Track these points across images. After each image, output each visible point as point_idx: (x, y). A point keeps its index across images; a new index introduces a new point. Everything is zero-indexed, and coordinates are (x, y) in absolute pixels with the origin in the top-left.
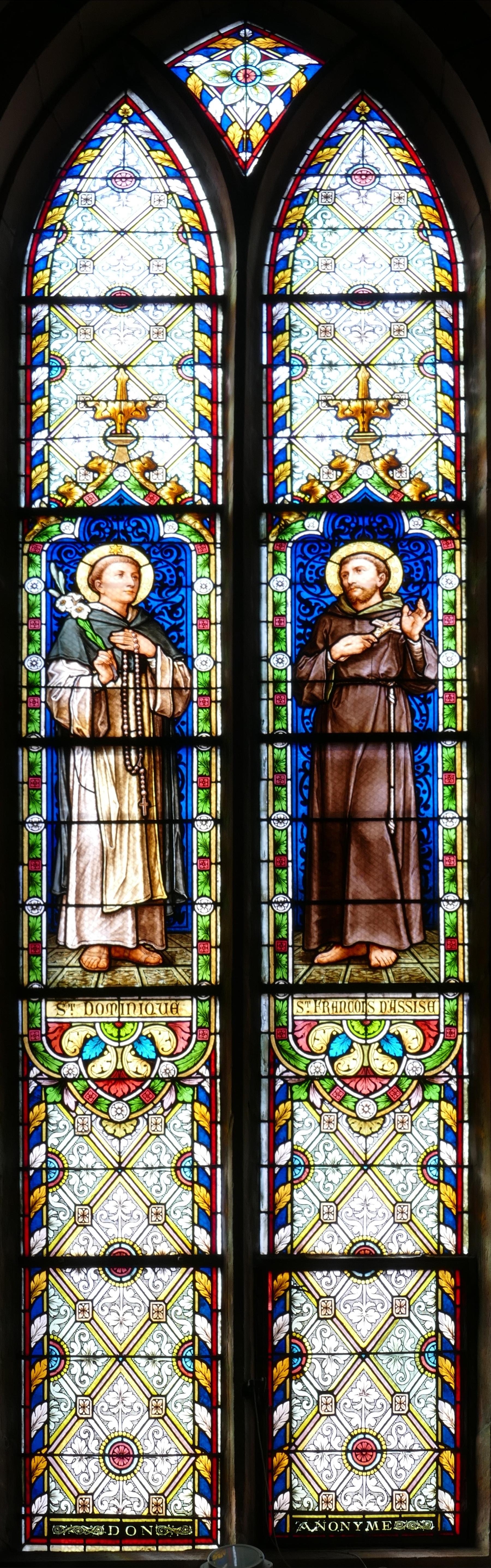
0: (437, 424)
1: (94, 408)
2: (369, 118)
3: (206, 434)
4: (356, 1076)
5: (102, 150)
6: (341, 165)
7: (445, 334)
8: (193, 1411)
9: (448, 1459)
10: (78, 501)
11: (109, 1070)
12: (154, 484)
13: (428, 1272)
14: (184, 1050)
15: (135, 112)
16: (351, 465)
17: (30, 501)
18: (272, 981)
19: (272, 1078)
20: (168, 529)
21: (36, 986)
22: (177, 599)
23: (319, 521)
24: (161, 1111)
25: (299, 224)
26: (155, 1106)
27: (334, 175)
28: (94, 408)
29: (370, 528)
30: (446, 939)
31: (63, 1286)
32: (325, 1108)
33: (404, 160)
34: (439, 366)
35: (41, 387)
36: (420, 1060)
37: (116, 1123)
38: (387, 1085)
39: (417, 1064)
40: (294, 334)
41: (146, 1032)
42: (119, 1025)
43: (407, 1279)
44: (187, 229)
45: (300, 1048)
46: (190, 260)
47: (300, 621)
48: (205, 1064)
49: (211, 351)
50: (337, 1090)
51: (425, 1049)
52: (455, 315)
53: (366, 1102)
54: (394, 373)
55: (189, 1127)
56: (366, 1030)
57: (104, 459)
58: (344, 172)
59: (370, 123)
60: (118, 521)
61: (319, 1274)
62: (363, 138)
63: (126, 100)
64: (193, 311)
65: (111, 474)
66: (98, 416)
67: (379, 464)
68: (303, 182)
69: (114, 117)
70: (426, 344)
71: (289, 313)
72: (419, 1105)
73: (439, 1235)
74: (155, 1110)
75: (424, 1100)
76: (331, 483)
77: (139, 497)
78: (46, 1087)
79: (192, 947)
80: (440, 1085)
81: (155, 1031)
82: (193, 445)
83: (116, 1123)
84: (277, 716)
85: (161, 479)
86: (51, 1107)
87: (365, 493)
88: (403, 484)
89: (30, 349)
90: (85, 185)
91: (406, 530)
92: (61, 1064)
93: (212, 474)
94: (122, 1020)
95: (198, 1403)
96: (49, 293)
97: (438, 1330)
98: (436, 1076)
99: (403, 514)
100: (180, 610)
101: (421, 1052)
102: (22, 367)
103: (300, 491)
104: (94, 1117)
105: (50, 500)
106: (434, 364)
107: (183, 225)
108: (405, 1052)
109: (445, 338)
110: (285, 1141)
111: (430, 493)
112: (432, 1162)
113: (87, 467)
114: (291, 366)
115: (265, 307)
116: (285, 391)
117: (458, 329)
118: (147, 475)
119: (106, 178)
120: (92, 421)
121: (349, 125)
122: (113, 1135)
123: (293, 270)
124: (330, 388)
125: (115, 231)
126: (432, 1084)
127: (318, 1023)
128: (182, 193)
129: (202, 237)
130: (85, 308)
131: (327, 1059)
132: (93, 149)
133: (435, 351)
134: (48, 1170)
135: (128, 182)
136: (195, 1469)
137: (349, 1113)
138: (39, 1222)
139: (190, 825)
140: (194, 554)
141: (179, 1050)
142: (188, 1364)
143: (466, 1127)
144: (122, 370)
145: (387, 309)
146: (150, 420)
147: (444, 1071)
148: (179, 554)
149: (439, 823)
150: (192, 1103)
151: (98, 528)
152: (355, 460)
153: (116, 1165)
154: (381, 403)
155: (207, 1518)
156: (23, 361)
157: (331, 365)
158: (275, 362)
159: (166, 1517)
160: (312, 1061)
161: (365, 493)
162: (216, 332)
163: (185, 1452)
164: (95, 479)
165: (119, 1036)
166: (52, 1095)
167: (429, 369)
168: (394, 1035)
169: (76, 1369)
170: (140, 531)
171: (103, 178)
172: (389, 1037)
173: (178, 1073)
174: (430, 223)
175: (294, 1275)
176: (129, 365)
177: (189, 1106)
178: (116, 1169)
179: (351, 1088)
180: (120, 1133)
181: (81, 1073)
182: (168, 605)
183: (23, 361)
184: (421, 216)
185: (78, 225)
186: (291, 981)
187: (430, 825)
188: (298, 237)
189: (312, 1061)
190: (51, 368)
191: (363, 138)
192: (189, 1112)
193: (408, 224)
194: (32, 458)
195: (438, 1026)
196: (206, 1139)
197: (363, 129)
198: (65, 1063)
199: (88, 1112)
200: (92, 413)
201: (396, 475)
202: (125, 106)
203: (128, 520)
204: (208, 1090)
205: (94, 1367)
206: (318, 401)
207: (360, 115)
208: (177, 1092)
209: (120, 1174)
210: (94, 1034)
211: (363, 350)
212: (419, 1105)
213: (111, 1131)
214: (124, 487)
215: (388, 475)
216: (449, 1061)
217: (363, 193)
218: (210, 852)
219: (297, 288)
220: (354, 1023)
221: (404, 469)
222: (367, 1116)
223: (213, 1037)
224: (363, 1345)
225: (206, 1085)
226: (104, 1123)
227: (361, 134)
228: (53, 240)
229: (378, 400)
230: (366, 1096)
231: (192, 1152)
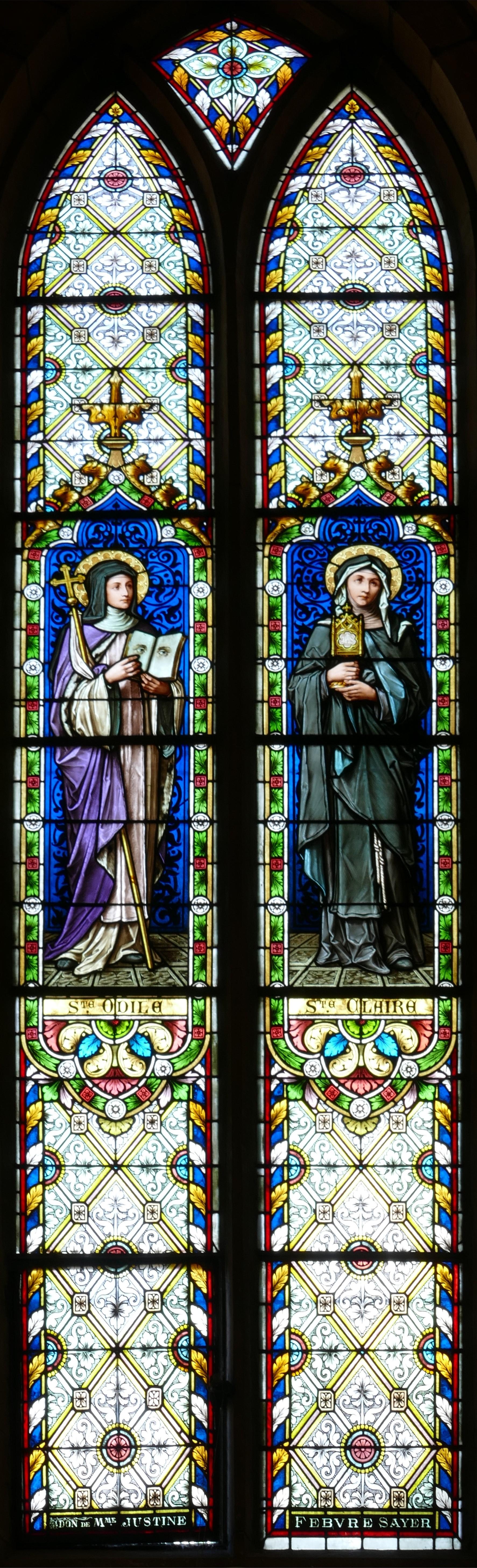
0: (188, 429)
1: (89, 412)
2: (358, 116)
3: (441, 432)
4: (103, 1078)
5: (93, 150)
6: (330, 164)
7: (437, 334)
8: (434, 1403)
9: (199, 1452)
10: (74, 504)
11: (351, 1068)
12: (391, 483)
13: (176, 1270)
14: (179, 1048)
15: (361, 107)
16: (344, 467)
17: (25, 504)
18: (268, 982)
19: (269, 1078)
20: (407, 530)
21: (31, 985)
22: (174, 602)
23: (314, 526)
24: (402, 1109)
25: (289, 224)
26: (396, 1104)
27: (87, 178)
28: (89, 412)
29: (366, 534)
30: (195, 942)
31: (306, 1279)
32: (75, 1109)
33: (393, 159)
34: (431, 367)
35: (276, 385)
36: (415, 1061)
37: (361, 1121)
38: (382, 1085)
39: (412, 1064)
40: (48, 338)
41: (141, 1030)
42: (360, 1023)
43: (157, 1277)
44: (179, 228)
45: (50, 1048)
46: (183, 260)
47: (297, 626)
48: (200, 1062)
49: (445, 348)
50: (87, 1090)
51: (420, 1049)
52: (446, 315)
53: (116, 1102)
54: (145, 378)
55: (184, 1125)
56: (361, 1030)
57: (99, 462)
58: (334, 171)
59: (359, 122)
60: (116, 525)
61: (73, 1271)
62: (352, 137)
63: (116, 100)
64: (426, 310)
65: (348, 475)
66: (93, 420)
67: (372, 465)
68: (56, 185)
69: (105, 117)
70: (418, 344)
71: (282, 313)
72: (169, 1104)
73: (189, 1234)
74: (151, 1108)
75: (173, 1099)
76: (83, 488)
77: (133, 499)
78: (42, 1086)
79: (189, 948)
80: (189, 1085)
81: (397, 1029)
82: (187, 447)
83: (357, 1120)
84: (272, 718)
85: (156, 482)
86: (47, 1105)
87: (117, 499)
88: (395, 485)
89: (263, 348)
90: (81, 186)
91: (401, 535)
92: (302, 1061)
93: (448, 472)
94: (364, 1017)
95: (440, 1394)
96: (44, 294)
97: (436, 1325)
98: (183, 1076)
99: (398, 519)
100: (177, 614)
101: (416, 1052)
102: (257, 366)
103: (294, 492)
104: (335, 1114)
105: (288, 499)
106: (426, 365)
107: (174, 225)
108: (154, 1052)
109: (436, 338)
110: (281, 1140)
111: (181, 498)
112: (428, 1161)
113: (81, 470)
114: (45, 370)
115: (257, 307)
116: (276, 391)
117: (260, 332)
118: (141, 478)
119: (99, 178)
120: (86, 425)
121: (340, 124)
122: (108, 1133)
123: (284, 269)
124: (83, 392)
125: (346, 227)
126: (181, 1084)
127: (66, 1023)
128: (410, 188)
129: (193, 237)
130: (316, 305)
131: (76, 1059)
132: (85, 149)
133: (187, 356)
134: (289, 1167)
135: (120, 182)
136: (192, 1459)
137: (345, 1113)
138: (35, 1218)
139: (430, 825)
140: (191, 558)
141: (175, 1048)
142: (429, 1357)
143: (215, 1126)
144: (116, 373)
145: (140, 314)
146: (144, 423)
147: (193, 1070)
148: (418, 555)
149: (190, 826)
150: (188, 1101)
151: (339, 529)
152: (348, 462)
153: (111, 1163)
154: (374, 404)
155: (202, 1507)
156: (257, 359)
157: (387, 365)
158: (30, 367)
159: (163, 1508)
160: (61, 1061)
161: (117, 499)
162: (450, 330)
163: (425, 1444)
164: (90, 483)
165: (361, 1033)
166: (49, 1093)
167: (181, 374)
168: (142, 1035)
169: (318, 1363)
170: (138, 536)
171: (331, 175)
172: (384, 1036)
173: (174, 1071)
174: (181, 225)
175: (48, 1272)
176: (124, 368)
177: (184, 1104)
178: (357, 1167)
179: (100, 1089)
180: (115, 1130)
181: (77, 1073)
182: (165, 610)
183: (257, 359)
184: (173, 219)
185: (309, 223)
186: (41, 982)
187: (181, 827)
188: (289, 236)
189: (61, 1061)
190: (285, 365)
191: (352, 137)
192: (183, 1110)
193: (397, 221)
194: (269, 457)
195: (432, 1025)
196: (447, 1137)
197: (352, 128)
198: (307, 1060)
199: (330, 1110)
200: (86, 417)
201: (147, 480)
202: (116, 106)
203: (127, 525)
204: (203, 1087)
205: (335, 1360)
206: (71, 405)
207: (349, 114)
208: (173, 1091)
209: (116, 1172)
210: (336, 1031)
211: (116, 356)
212: (169, 1104)
213: (107, 1129)
214: (361, 487)
215: (379, 475)
216: (197, 1061)
217: (116, 195)
218: (451, 851)
219: (290, 288)
220: (349, 1023)
221: (154, 474)
222: (360, 1116)
223: (454, 1036)
224: (362, 1342)
225: (201, 1083)
226: (101, 1121)
227: (350, 133)
228: (46, 242)
229: (371, 400)
230: (115, 1097)
231: (187, 1150)
